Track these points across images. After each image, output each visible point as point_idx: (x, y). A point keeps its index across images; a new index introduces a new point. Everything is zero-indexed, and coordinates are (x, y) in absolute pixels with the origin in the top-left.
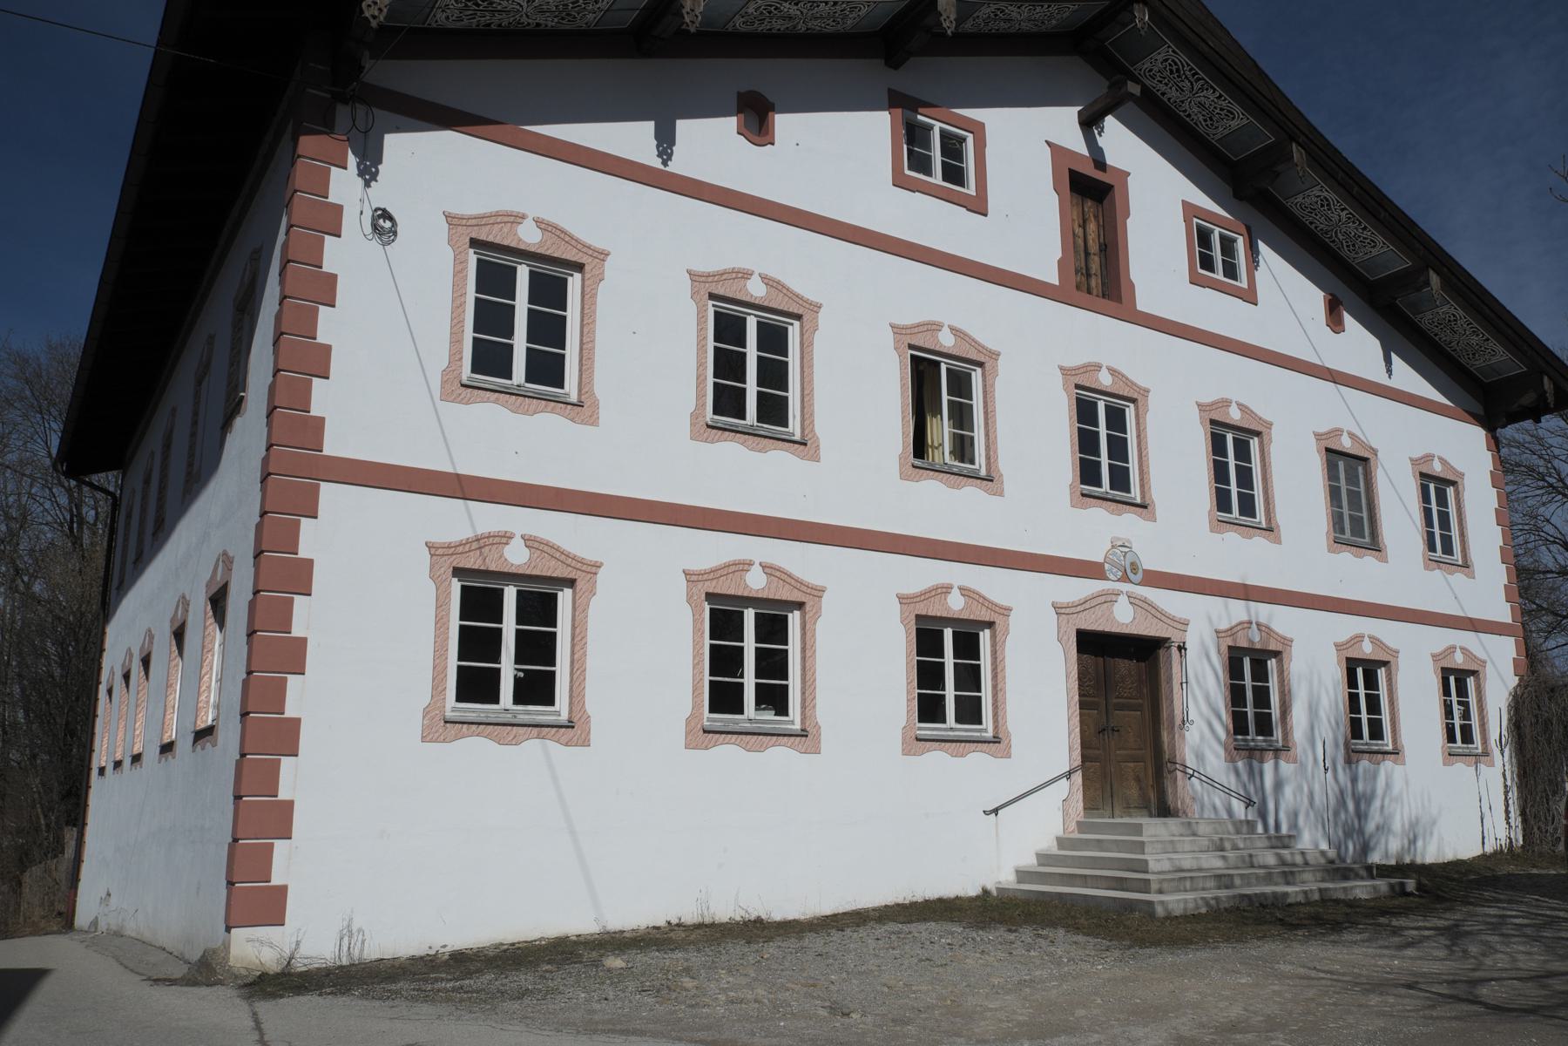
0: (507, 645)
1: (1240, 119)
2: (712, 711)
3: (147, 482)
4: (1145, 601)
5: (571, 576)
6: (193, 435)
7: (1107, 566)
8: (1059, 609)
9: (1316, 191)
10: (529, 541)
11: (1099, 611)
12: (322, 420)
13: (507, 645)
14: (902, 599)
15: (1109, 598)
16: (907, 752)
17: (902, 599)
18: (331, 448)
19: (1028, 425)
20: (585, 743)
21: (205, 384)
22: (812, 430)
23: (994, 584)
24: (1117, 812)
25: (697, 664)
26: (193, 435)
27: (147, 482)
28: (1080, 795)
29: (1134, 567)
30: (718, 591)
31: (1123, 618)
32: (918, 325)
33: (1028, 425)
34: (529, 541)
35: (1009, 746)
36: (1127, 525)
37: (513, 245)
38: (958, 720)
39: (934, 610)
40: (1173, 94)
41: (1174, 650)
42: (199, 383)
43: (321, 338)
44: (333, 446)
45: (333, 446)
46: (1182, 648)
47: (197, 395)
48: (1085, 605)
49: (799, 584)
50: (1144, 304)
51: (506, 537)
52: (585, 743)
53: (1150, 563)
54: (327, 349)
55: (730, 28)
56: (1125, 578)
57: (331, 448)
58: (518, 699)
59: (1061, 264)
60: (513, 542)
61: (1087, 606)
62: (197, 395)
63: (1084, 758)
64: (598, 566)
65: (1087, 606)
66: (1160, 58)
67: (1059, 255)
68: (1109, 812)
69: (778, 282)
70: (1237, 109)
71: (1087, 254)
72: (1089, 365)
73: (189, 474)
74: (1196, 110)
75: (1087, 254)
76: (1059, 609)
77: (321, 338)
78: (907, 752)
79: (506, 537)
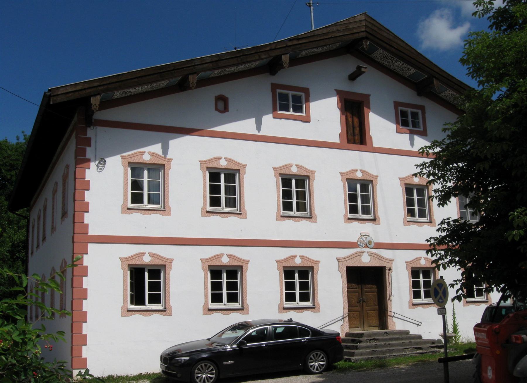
0: (146, 285)
1: (413, 71)
3: (39, 218)
5: (164, 264)
6: (53, 213)
7: (358, 243)
8: (339, 260)
9: (448, 92)
10: (151, 254)
12: (88, 224)
13: (146, 285)
14: (278, 262)
15: (360, 254)
17: (278, 262)
18: (91, 233)
19: (328, 196)
20: (171, 314)
21: (55, 196)
22: (244, 208)
23: (313, 254)
25: (345, 200)
26: (53, 213)
27: (39, 218)
28: (348, 324)
29: (370, 243)
30: (212, 264)
31: (366, 260)
32: (283, 166)
33: (328, 196)
35: (319, 308)
36: (367, 228)
37: (142, 162)
39: (290, 264)
40: (386, 63)
41: (387, 272)
42: (54, 195)
43: (86, 200)
44: (92, 232)
45: (92, 232)
46: (390, 270)
47: (53, 199)
48: (349, 257)
49: (240, 260)
50: (376, 144)
52: (171, 314)
53: (376, 240)
54: (88, 203)
55: (211, 76)
56: (367, 246)
57: (91, 233)
58: (229, 301)
59: (340, 135)
60: (145, 255)
61: (350, 258)
62: (53, 199)
63: (349, 310)
64: (172, 260)
65: (350, 258)
66: (379, 53)
67: (340, 131)
69: (231, 159)
70: (411, 68)
71: (354, 127)
72: (352, 170)
73: (52, 228)
74: (396, 68)
75: (354, 127)
76: (339, 260)
77: (86, 200)
79: (143, 254)
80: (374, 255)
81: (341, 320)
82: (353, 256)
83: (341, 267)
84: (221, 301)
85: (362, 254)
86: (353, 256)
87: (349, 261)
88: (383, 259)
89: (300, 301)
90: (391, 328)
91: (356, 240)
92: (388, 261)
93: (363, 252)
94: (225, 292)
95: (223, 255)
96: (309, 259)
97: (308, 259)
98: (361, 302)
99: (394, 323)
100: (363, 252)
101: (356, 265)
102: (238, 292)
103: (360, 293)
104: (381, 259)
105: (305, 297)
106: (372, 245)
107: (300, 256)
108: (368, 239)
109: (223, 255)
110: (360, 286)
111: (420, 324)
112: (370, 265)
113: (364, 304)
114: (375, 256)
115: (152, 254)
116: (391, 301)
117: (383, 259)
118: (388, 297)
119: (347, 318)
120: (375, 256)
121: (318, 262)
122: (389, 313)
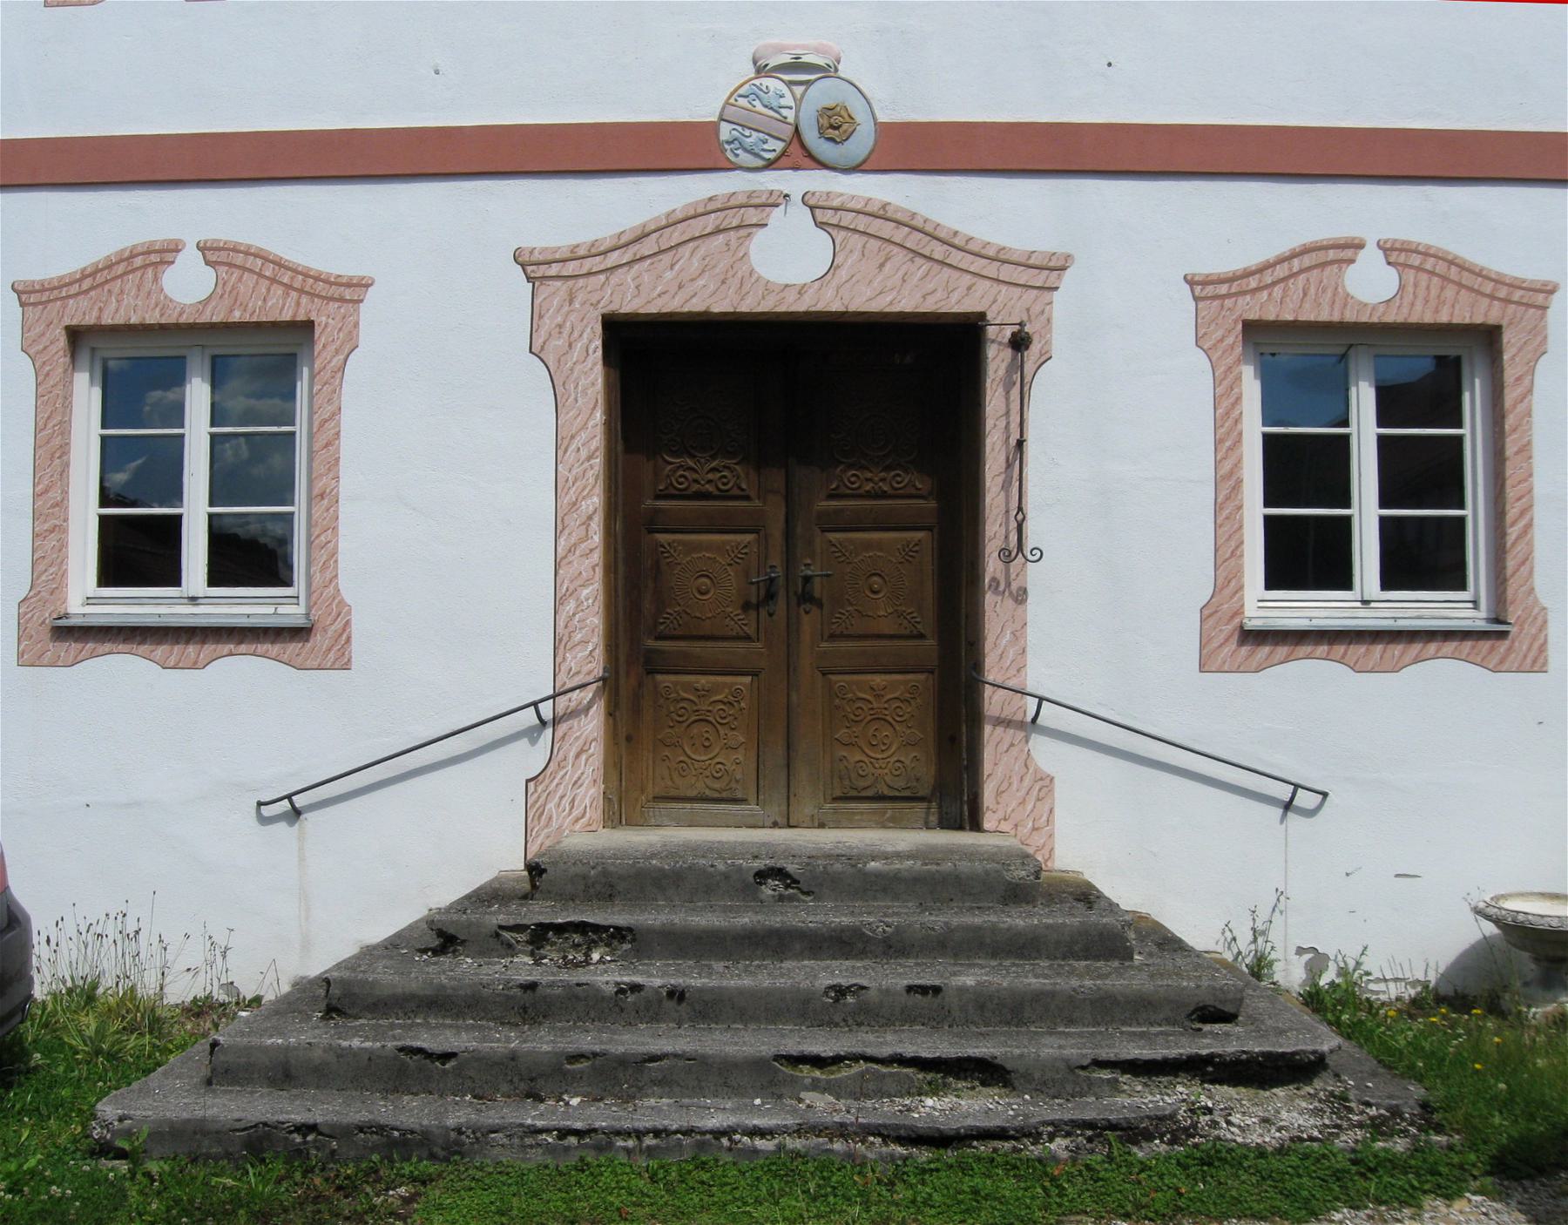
2: (1269, 585)
4: (882, 214)
5: (1492, 319)
7: (726, 131)
10: (1394, 252)
11: (690, 260)
14: (27, 294)
15: (741, 219)
16: (27, 658)
17: (27, 294)
20: (1536, 662)
24: (806, 808)
29: (835, 124)
31: (790, 264)
34: (1394, 252)
38: (1388, 582)
41: (997, 359)
48: (636, 245)
51: (162, 255)
53: (895, 94)
56: (797, 153)
58: (1392, 578)
60: (180, 258)
61: (648, 247)
64: (1549, 290)
65: (648, 247)
68: (775, 811)
78: (27, 658)
80: (876, 226)
81: (532, 734)
82: (676, 235)
83: (547, 324)
84: (1337, 574)
85: (752, 216)
86: (676, 235)
87: (628, 276)
88: (955, 257)
89: (214, 580)
90: (1003, 826)
91: (706, 111)
92: (1007, 272)
93: (773, 201)
94: (1366, 513)
95: (174, 248)
96: (279, 264)
97: (273, 269)
98: (781, 605)
99: (1045, 783)
100: (773, 201)
101: (696, 305)
102: (1467, 512)
103: (776, 530)
104: (938, 251)
105: (1422, 558)
106: (861, 143)
107: (203, 248)
108: (822, 93)
109: (174, 248)
110: (776, 479)
111: (1305, 800)
112: (831, 301)
113: (809, 622)
114: (887, 229)
115: (1406, 248)
116: (1021, 597)
117: (955, 257)
118: (992, 566)
119: (592, 725)
120: (887, 229)
121: (349, 291)
122: (994, 702)
